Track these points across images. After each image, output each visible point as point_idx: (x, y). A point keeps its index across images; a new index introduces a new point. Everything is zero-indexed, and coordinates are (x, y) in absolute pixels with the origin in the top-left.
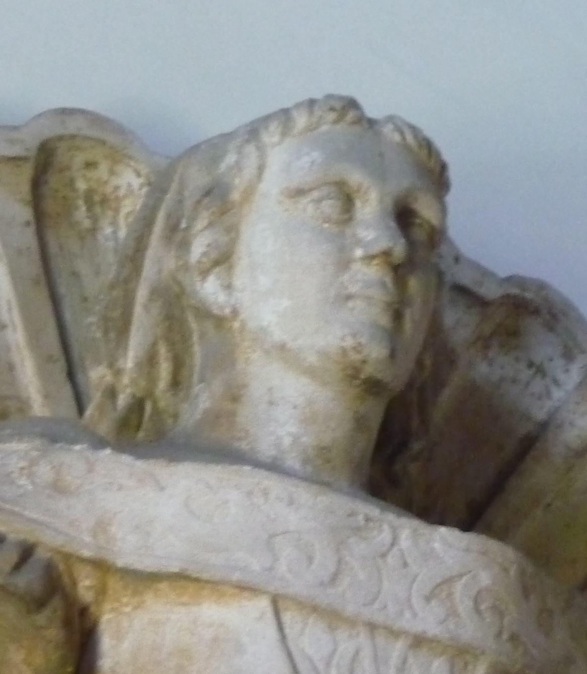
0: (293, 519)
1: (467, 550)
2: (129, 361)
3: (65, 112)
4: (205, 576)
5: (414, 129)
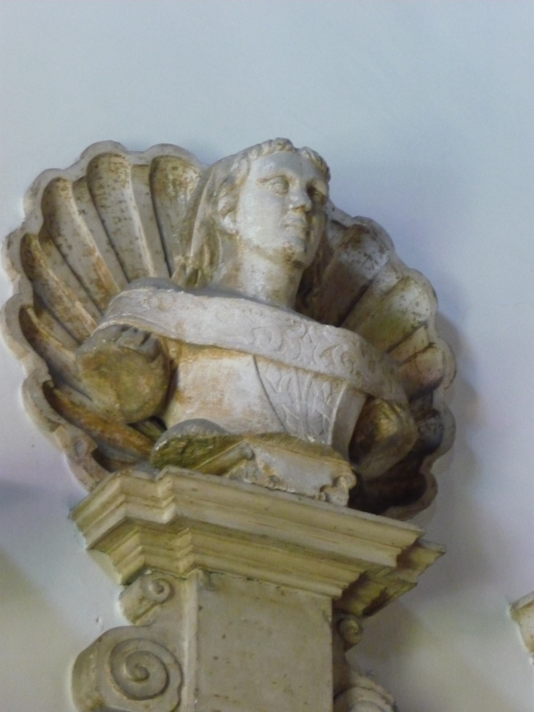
0: (262, 322)
1: (338, 335)
2: (191, 254)
3: (164, 146)
4: (224, 346)
5: (315, 153)
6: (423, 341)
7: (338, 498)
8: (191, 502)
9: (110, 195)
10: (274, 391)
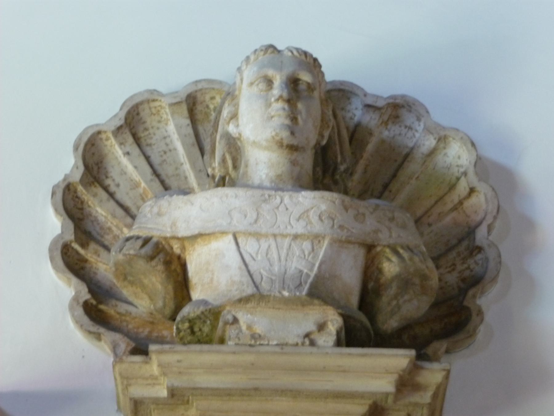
1: (314, 198)
2: (216, 164)
3: (197, 82)
4: (207, 232)
5: (297, 50)
6: (465, 188)
7: (324, 341)
8: (180, 373)
9: (154, 134)
10: (254, 259)
